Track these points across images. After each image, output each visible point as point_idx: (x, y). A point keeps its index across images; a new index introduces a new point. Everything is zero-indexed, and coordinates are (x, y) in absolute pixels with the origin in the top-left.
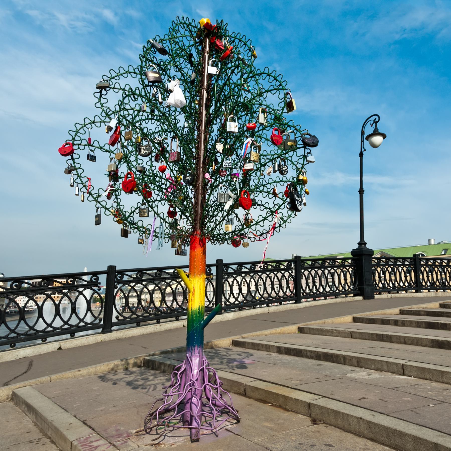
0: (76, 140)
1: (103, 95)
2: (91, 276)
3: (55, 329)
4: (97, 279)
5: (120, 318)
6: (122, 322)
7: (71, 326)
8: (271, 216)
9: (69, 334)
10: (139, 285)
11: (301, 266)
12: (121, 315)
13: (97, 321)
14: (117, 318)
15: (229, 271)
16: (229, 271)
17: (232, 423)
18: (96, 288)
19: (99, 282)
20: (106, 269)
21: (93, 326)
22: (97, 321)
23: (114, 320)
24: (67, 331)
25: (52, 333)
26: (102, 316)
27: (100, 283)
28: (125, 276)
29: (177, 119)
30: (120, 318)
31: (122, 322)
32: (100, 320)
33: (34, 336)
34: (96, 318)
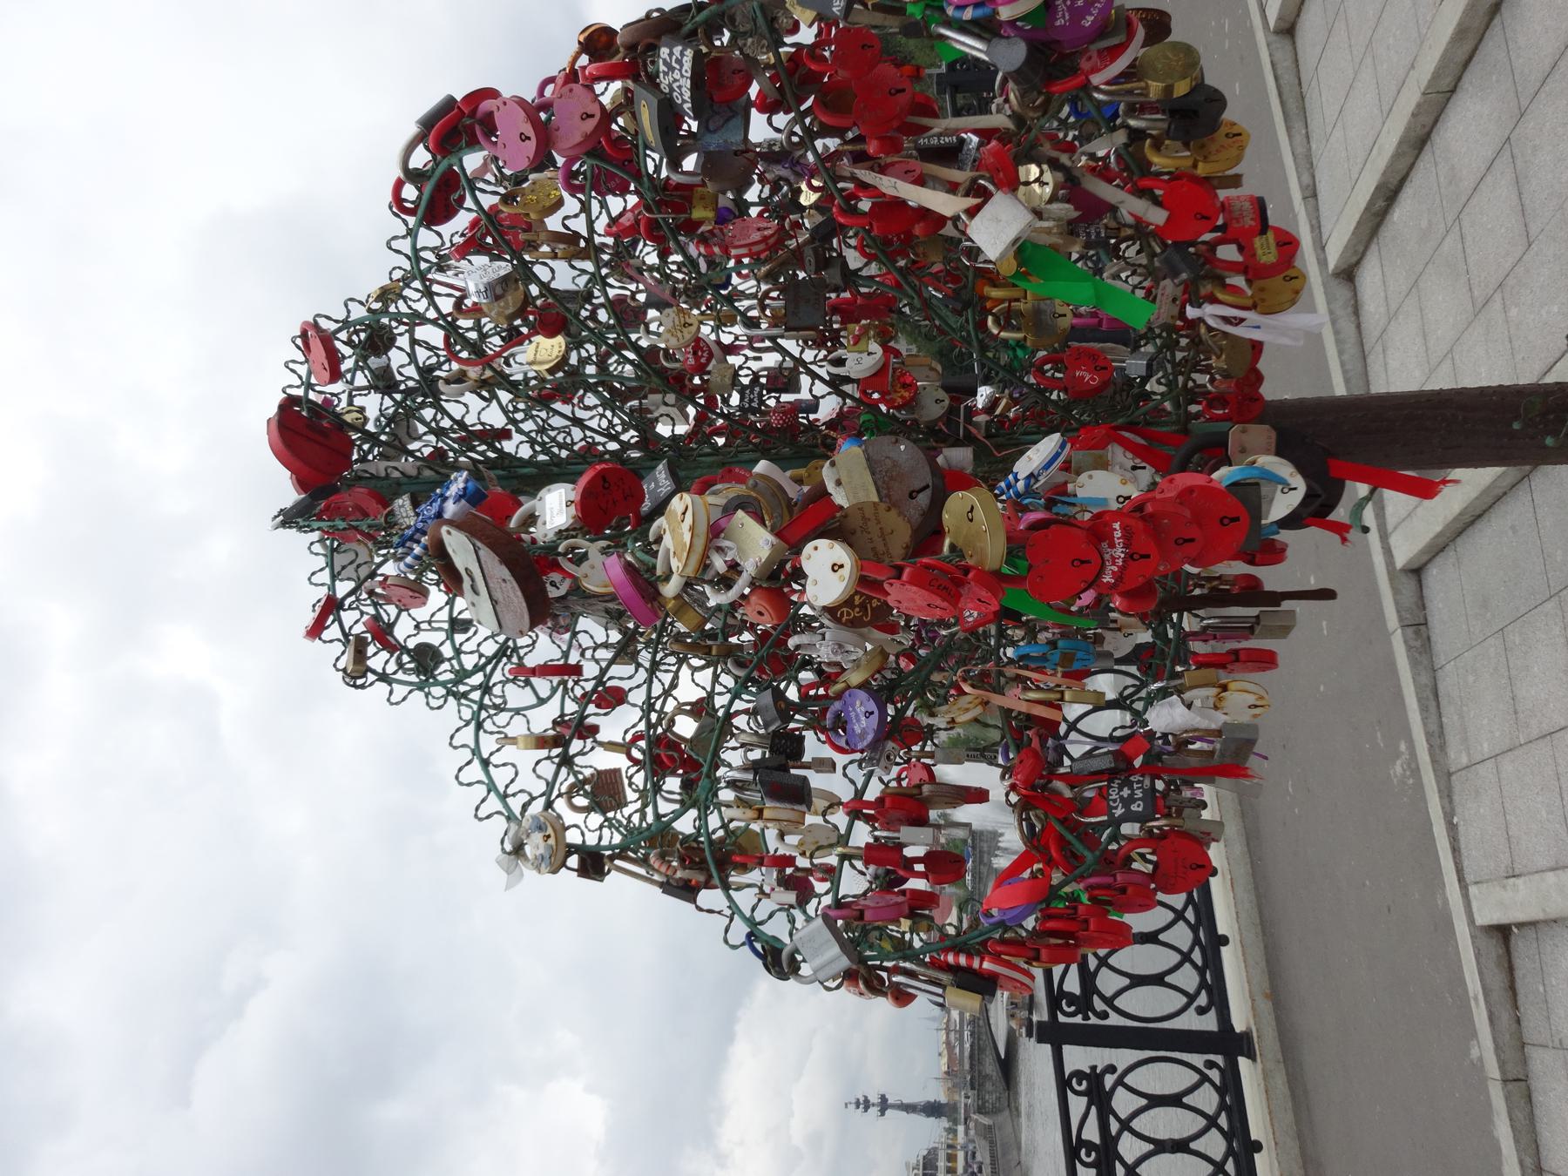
0: (584, 841)
1: (409, 364)
2: (1078, 1165)
3: (1222, 1106)
4: (1079, 1075)
5: (1202, 1000)
6: (1216, 998)
7: (1230, 1152)
8: (843, 831)
9: (1219, 952)
10: (1114, 1104)
11: (968, 69)
12: (1191, 998)
13: (1214, 1075)
14: (1202, 1011)
15: (1077, 990)
16: (1077, 990)
17: (1369, 60)
18: (1109, 1080)
19: (1088, 1071)
20: (1047, 1048)
21: (1231, 1088)
22: (1214, 1075)
23: (1209, 1023)
24: (1209, 952)
25: (1209, 952)
26: (1197, 1060)
27: (1094, 1068)
28: (1084, 1136)
29: (445, 698)
30: (1202, 1000)
31: (1216, 998)
32: (1211, 1065)
33: (1215, 991)
34: (1205, 1078)
